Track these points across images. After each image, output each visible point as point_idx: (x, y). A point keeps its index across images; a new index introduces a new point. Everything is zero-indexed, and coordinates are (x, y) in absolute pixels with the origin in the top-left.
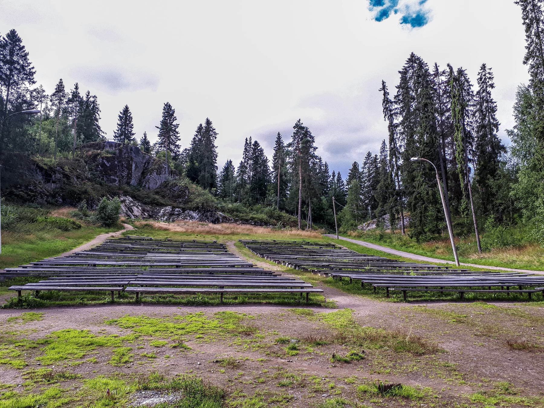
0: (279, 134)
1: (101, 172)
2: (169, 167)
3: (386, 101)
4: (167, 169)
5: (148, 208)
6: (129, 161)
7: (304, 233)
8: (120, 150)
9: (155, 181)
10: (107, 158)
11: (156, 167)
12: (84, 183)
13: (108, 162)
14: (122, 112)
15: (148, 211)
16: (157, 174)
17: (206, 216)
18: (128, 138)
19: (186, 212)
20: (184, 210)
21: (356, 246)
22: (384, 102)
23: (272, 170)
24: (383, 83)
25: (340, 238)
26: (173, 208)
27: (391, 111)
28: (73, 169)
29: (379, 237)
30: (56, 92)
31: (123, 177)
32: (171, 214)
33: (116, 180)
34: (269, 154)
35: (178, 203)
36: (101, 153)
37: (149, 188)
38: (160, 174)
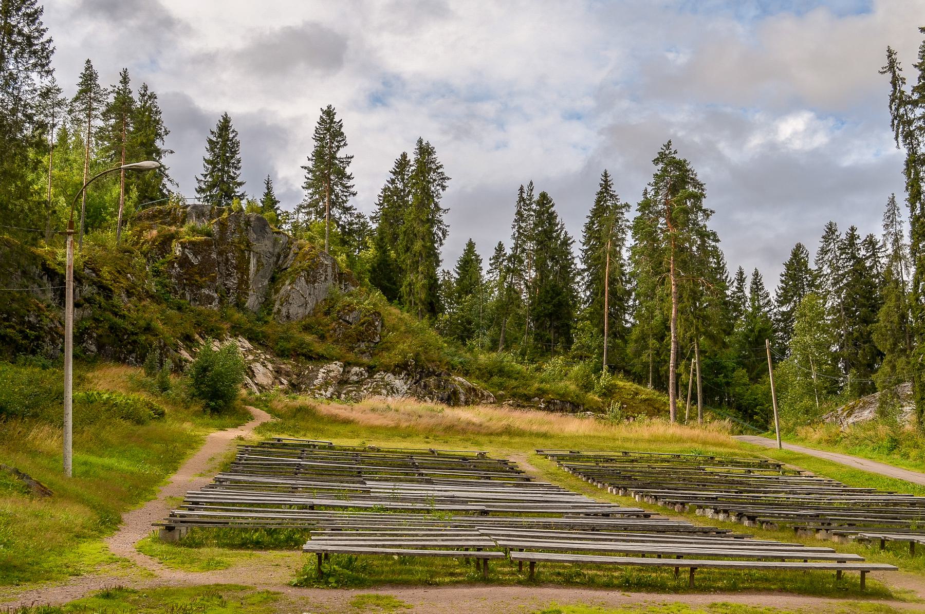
0: (606, 175)
1: (179, 277)
2: (335, 263)
3: (899, 100)
4: (329, 270)
5: (287, 365)
6: (243, 251)
7: (684, 431)
8: (222, 225)
9: (298, 299)
10: (193, 244)
11: (306, 264)
12: (144, 306)
13: (195, 255)
14: (215, 130)
15: (288, 374)
16: (307, 282)
17: (425, 386)
18: (228, 194)
19: (377, 376)
20: (371, 370)
21: (833, 469)
22: (892, 101)
23: (581, 266)
24: (890, 53)
25: (785, 445)
26: (347, 365)
27: (910, 122)
28: (119, 272)
29: (886, 443)
30: (81, 92)
31: (229, 289)
32: (343, 382)
33: (213, 299)
34: (574, 226)
35: (363, 352)
36: (177, 233)
37: (288, 317)
38: (315, 282)
